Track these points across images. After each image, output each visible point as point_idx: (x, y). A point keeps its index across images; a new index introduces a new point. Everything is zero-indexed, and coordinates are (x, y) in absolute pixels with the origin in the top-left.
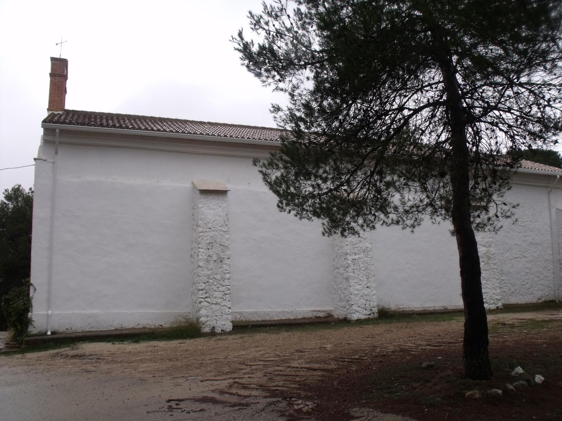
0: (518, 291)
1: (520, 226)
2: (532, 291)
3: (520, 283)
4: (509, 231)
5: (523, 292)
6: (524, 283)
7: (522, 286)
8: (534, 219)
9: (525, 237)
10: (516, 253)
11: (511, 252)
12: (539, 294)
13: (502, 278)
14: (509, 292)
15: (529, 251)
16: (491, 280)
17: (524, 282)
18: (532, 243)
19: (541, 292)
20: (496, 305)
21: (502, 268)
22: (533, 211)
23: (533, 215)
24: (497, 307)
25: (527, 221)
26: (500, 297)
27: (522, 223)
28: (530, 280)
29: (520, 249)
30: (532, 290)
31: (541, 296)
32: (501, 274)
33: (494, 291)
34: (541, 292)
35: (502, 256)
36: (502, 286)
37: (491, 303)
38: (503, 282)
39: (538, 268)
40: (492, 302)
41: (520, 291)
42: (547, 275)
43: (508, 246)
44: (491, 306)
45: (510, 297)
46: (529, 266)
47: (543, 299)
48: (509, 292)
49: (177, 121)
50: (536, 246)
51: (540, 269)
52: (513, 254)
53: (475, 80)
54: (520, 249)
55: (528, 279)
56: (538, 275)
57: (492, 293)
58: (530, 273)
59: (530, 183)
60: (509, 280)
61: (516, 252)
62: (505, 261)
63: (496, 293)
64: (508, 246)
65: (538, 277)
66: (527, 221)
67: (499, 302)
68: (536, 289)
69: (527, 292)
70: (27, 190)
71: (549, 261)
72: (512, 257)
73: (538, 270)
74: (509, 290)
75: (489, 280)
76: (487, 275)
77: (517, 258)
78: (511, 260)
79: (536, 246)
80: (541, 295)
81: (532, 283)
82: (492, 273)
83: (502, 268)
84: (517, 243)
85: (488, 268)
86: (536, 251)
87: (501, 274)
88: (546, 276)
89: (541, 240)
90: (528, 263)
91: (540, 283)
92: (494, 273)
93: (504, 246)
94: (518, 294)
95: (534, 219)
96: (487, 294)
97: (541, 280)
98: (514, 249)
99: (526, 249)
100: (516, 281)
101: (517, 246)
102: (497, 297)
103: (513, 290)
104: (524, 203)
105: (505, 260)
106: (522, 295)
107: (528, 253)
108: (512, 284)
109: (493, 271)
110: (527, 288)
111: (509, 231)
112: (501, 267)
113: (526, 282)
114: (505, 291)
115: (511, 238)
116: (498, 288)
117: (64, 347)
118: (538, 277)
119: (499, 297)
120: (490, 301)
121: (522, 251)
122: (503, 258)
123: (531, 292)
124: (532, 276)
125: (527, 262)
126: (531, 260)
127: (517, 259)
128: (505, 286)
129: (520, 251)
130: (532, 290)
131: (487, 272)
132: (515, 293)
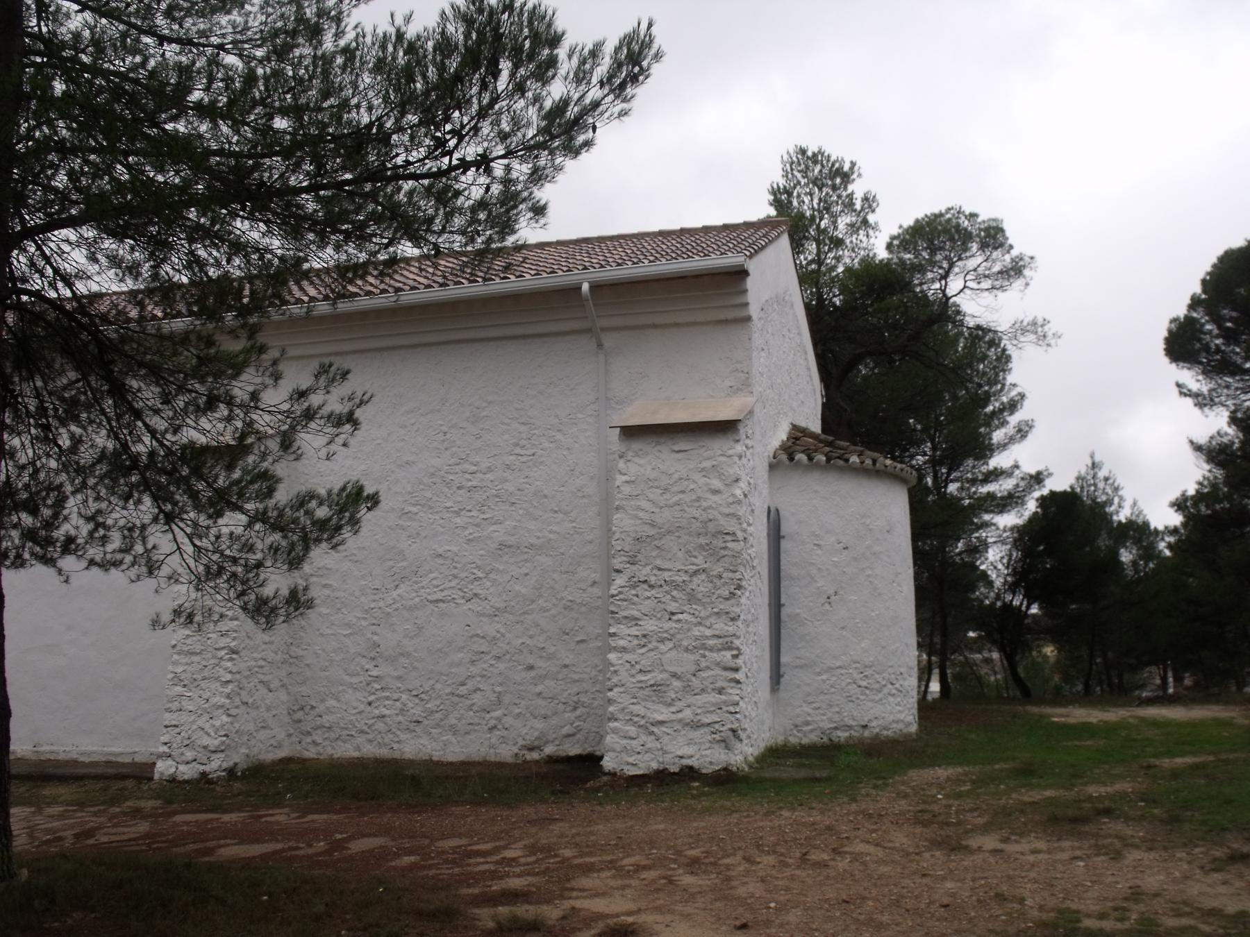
0: (438, 716)
1: (459, 488)
2: (499, 719)
3: (448, 690)
4: (414, 509)
5: (459, 719)
6: (463, 690)
7: (455, 699)
8: (524, 459)
9: (477, 525)
10: (437, 586)
11: (416, 582)
12: (530, 730)
13: (375, 673)
14: (400, 718)
15: (492, 576)
16: (204, 684)
17: (463, 684)
18: (510, 546)
19: (539, 725)
20: (202, 768)
21: (375, 638)
22: (522, 428)
23: (523, 442)
24: (204, 775)
25: (490, 470)
26: (216, 742)
27: (468, 476)
28: (492, 681)
29: (455, 571)
30: (498, 713)
31: (538, 738)
32: (373, 659)
33: (201, 722)
34: (539, 725)
35: (377, 597)
36: (372, 698)
37: (184, 758)
38: (377, 686)
39: (531, 637)
40: (189, 755)
41: (446, 716)
42: (567, 662)
43: (404, 564)
44: (182, 768)
45: (403, 736)
46: (491, 629)
47: (549, 750)
48: (400, 718)
49: (601, 240)
50: (526, 556)
51: (541, 639)
52: (423, 587)
53: (77, 54)
54: (455, 571)
55: (483, 676)
56: (531, 660)
57: (194, 727)
58: (493, 653)
59: (681, 318)
60: (399, 678)
61: (435, 582)
62: (389, 614)
63: (207, 726)
64: (404, 564)
65: (531, 668)
66: (490, 470)
67: (214, 756)
68: (518, 711)
69: (476, 720)
70: (1010, 379)
71: (583, 609)
72: (417, 600)
73: (528, 641)
74: (402, 711)
75: (196, 683)
76: (189, 669)
77: (437, 601)
78: (410, 609)
79: (526, 556)
80: (536, 734)
81: (498, 689)
82: (212, 661)
83: (375, 638)
84: (440, 551)
85: (198, 648)
86: (527, 574)
87: (373, 659)
88: (566, 666)
89: (551, 532)
90: (485, 620)
91: (539, 689)
92: (217, 661)
93: (391, 563)
94: (438, 726)
95: (524, 459)
96: (178, 730)
97: (543, 678)
98: (431, 572)
99: (478, 567)
100: (432, 682)
101: (440, 561)
102: (206, 741)
103: (417, 711)
104: (485, 405)
105: (388, 610)
106: (453, 730)
107: (489, 584)
108: (415, 693)
109: (214, 657)
110: (475, 708)
111: (414, 509)
112: (369, 635)
113: (470, 685)
114: (384, 716)
115: (418, 534)
116: (221, 711)
117: (1215, 708)
118: (531, 668)
119: (214, 743)
120: (182, 754)
121: (463, 575)
122: (381, 604)
123: (493, 722)
124: (502, 666)
125: (480, 614)
126: (498, 609)
127: (442, 605)
128: (387, 698)
129: (455, 577)
130: (498, 713)
131: (196, 659)
132: (426, 722)
